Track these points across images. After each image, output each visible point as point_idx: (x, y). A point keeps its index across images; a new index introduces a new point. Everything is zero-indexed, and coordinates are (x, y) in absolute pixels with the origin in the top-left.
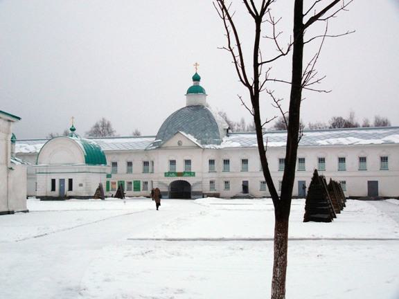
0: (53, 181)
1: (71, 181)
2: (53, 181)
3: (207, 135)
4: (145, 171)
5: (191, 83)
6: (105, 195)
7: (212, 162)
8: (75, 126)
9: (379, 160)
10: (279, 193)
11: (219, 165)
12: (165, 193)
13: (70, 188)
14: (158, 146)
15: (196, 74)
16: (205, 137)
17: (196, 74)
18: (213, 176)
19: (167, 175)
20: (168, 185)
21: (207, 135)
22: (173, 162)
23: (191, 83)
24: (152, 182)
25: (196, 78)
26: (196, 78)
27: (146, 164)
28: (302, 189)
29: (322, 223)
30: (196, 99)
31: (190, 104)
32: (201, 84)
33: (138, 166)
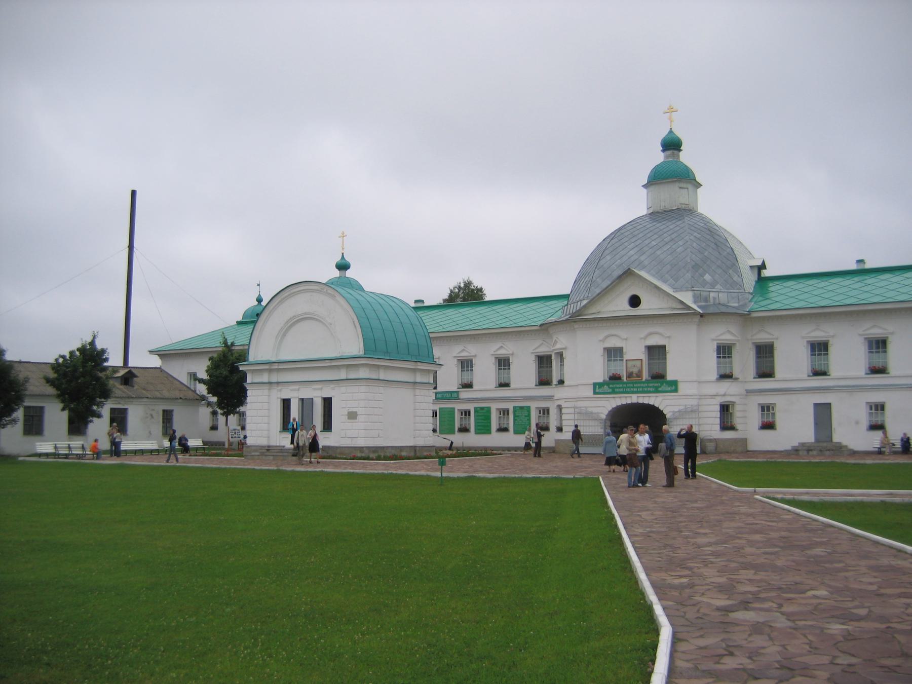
0: (286, 403)
1: (327, 402)
2: (286, 403)
3: (707, 277)
4: (544, 381)
5: (659, 157)
6: (806, 433)
7: (724, 351)
8: (347, 258)
9: (778, 424)
10: (20, 459)
11: (744, 362)
12: (105, 452)
13: (328, 425)
14: (576, 319)
15: (671, 131)
16: (705, 283)
17: (671, 131)
18: (729, 391)
19: (598, 388)
20: (604, 417)
21: (707, 277)
22: (613, 353)
23: (659, 157)
24: (560, 408)
25: (672, 145)
26: (672, 145)
27: (544, 361)
28: (393, 452)
29: (782, 449)
30: (671, 196)
31: (657, 209)
32: (686, 157)
33: (524, 373)
